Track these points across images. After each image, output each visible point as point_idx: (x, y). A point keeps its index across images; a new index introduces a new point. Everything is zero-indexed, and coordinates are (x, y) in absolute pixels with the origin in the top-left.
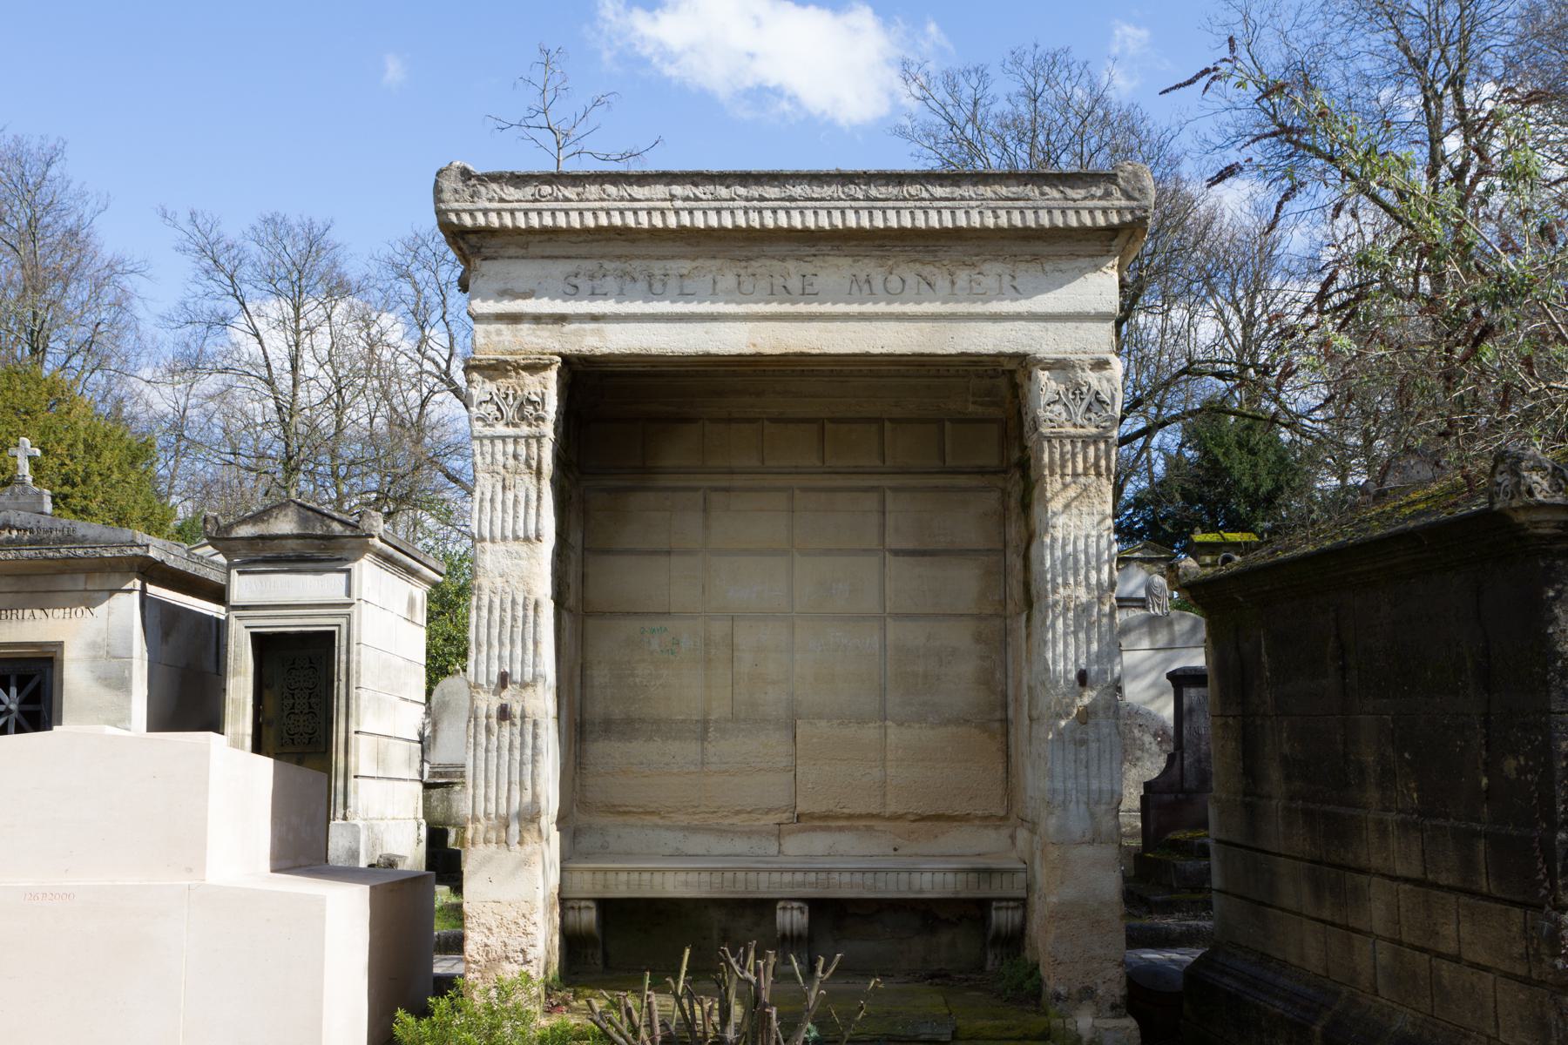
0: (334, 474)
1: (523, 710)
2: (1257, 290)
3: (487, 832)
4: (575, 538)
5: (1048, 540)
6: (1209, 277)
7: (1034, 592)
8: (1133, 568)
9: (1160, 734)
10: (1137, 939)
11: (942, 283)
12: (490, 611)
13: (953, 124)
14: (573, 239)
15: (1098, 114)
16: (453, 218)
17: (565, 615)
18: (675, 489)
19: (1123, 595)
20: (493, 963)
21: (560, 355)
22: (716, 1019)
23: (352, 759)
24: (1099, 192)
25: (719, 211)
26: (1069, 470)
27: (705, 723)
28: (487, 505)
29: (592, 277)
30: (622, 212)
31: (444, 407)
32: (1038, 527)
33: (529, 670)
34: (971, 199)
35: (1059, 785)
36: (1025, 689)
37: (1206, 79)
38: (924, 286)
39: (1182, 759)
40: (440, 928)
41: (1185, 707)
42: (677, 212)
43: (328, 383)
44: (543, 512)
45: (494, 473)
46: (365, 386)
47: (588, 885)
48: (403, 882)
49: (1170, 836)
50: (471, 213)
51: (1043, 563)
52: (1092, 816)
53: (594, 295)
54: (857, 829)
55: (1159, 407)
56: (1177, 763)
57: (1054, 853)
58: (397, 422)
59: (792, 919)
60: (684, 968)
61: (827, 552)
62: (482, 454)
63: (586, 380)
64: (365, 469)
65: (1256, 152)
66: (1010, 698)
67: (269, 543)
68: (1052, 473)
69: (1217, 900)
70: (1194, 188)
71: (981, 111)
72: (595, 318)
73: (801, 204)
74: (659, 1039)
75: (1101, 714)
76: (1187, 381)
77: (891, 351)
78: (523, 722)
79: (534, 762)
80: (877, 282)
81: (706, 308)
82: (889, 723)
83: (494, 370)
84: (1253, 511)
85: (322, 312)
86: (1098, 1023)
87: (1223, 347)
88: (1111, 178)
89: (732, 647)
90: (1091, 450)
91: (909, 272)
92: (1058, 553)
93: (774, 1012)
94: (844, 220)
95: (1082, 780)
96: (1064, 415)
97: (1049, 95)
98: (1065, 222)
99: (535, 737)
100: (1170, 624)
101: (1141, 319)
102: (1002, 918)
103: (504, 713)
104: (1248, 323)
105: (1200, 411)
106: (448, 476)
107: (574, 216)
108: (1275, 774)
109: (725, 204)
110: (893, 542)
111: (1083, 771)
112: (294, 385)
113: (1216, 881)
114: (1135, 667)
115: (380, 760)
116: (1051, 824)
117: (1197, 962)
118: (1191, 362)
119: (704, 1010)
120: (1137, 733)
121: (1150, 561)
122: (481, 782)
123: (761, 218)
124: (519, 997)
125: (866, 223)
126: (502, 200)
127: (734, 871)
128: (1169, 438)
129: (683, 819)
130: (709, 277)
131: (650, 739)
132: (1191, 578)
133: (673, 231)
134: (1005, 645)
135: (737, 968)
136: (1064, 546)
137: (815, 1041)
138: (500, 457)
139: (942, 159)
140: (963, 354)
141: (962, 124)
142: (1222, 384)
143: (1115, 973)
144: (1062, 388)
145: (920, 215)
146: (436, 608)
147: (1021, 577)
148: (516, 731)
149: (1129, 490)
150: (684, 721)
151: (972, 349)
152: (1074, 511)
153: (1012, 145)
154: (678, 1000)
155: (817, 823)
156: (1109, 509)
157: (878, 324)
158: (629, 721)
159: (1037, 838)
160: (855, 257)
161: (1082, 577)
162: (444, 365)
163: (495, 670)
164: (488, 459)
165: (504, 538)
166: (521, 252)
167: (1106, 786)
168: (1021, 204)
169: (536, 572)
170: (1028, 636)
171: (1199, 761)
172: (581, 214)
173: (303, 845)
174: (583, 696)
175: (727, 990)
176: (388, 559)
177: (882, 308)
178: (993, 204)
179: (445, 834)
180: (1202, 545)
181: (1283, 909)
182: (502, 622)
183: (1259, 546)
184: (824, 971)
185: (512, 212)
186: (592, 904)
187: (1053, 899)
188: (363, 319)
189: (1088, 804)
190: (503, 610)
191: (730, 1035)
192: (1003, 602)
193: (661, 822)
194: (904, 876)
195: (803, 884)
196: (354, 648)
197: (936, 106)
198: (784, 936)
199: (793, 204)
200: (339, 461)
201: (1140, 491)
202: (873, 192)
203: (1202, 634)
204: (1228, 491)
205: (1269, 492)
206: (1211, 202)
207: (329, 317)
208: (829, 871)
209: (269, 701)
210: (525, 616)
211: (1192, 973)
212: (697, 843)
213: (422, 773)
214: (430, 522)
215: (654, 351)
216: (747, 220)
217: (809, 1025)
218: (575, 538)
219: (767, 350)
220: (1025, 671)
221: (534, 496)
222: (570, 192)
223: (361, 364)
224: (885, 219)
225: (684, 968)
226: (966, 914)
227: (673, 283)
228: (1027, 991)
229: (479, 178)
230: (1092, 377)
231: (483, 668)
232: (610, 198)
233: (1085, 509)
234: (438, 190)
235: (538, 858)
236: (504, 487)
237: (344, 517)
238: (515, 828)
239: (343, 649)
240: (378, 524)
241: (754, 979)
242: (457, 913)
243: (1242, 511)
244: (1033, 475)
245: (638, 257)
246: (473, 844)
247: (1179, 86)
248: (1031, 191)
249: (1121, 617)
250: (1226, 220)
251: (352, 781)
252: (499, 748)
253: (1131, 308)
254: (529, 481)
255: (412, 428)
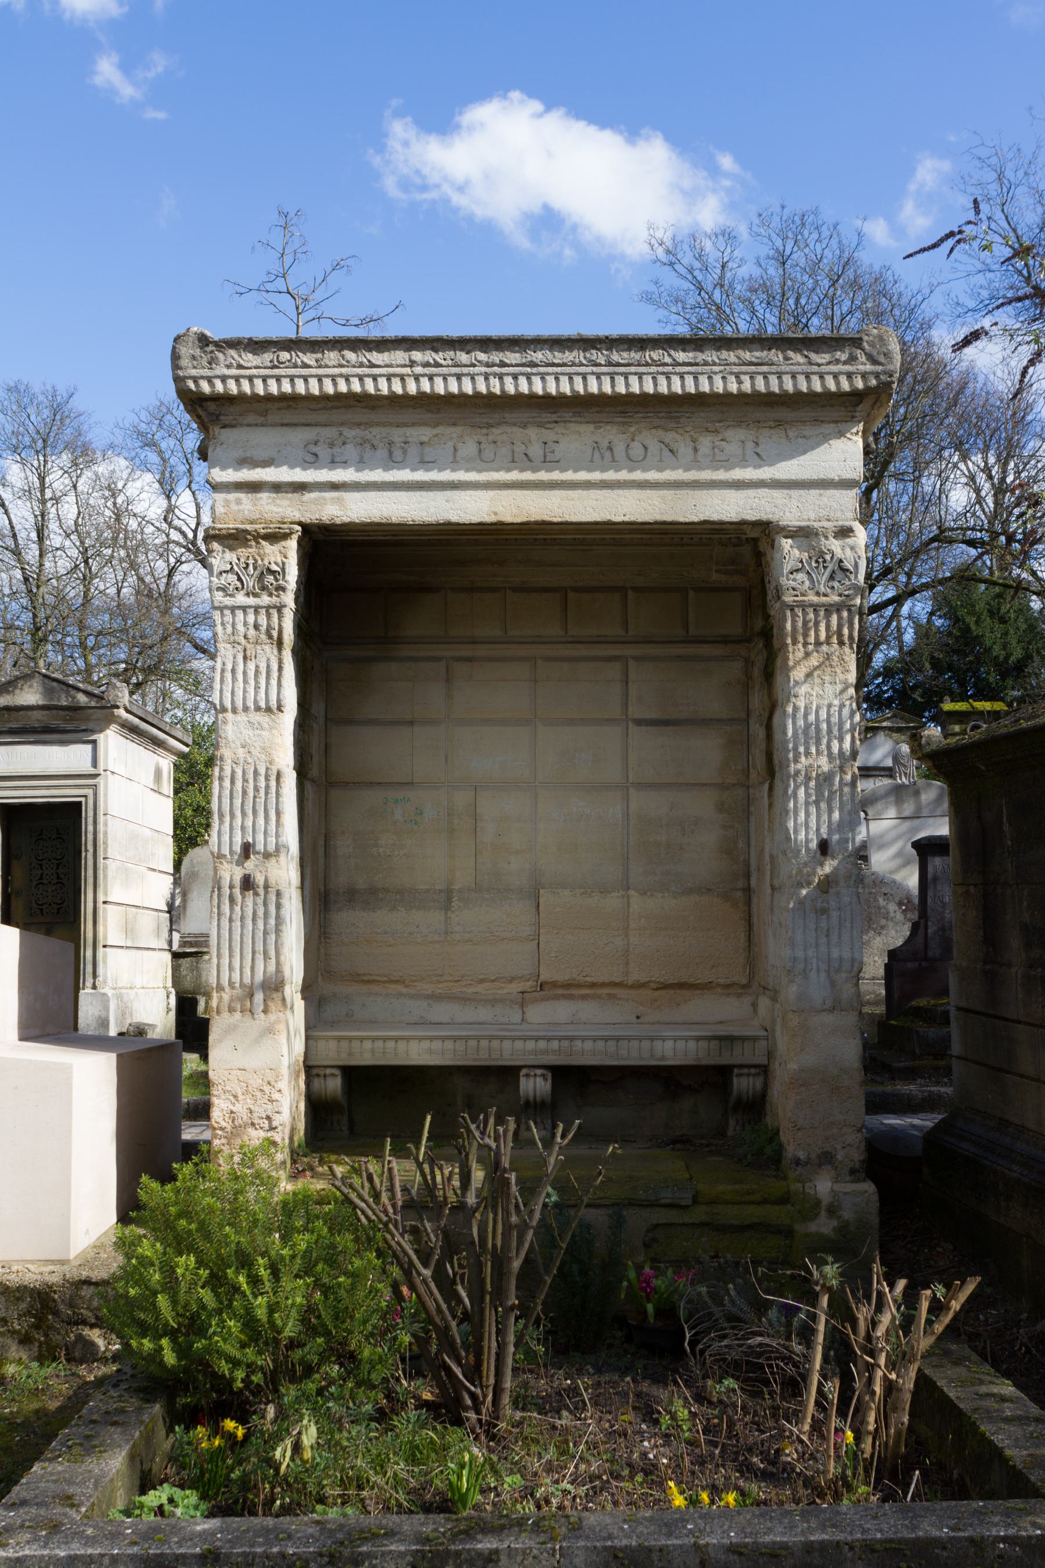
0: (83, 645)
1: (266, 880)
2: (1009, 457)
3: (232, 1000)
4: (318, 708)
5: (790, 709)
6: (961, 443)
7: (776, 761)
8: (881, 737)
9: (905, 902)
10: (876, 1105)
11: (685, 449)
12: (233, 782)
13: (701, 289)
14: (313, 406)
15: (844, 274)
16: (191, 385)
17: (308, 786)
18: (417, 659)
19: (870, 764)
20: (237, 1130)
21: (300, 524)
22: (456, 1183)
23: (101, 929)
24: (844, 357)
25: (459, 377)
26: (812, 639)
27: (448, 893)
28: (228, 675)
29: (332, 445)
30: (361, 378)
31: (193, 578)
32: (780, 697)
33: (272, 840)
34: (714, 364)
35: (800, 954)
36: (767, 858)
37: (951, 242)
38: (666, 453)
39: (926, 927)
40: (187, 1095)
41: (930, 876)
42: (417, 378)
43: (74, 553)
44: (284, 682)
45: (235, 643)
46: (112, 556)
47: (334, 1052)
48: (150, 1050)
49: (914, 1003)
50: (209, 380)
51: (785, 733)
52: (833, 983)
53: (333, 463)
54: (600, 997)
55: (909, 576)
56: (921, 931)
57: (794, 1020)
58: (144, 592)
59: (535, 1086)
60: (426, 1135)
61: (571, 722)
62: (223, 624)
63: (328, 552)
64: (113, 640)
65: (1006, 317)
66: (753, 868)
67: (14, 714)
68: (795, 642)
69: (956, 1067)
70: (945, 352)
71: (728, 275)
72: (335, 486)
73: (542, 370)
74: (400, 1203)
75: (842, 883)
76: (937, 549)
77: (633, 519)
78: (266, 893)
79: (278, 931)
80: (620, 449)
81: (446, 476)
82: (632, 892)
83: (234, 539)
84: (1003, 679)
85: (67, 481)
86: (836, 1187)
87: (974, 514)
88: (856, 342)
89: (475, 817)
90: (834, 618)
91: (651, 439)
92: (801, 723)
93: (513, 1177)
94: (585, 386)
95: (823, 949)
96: (807, 583)
97: (799, 257)
98: (809, 387)
99: (278, 906)
100: (917, 793)
101: (892, 486)
102: (743, 1085)
103: (247, 883)
104: (1000, 490)
105: (950, 578)
106: (196, 647)
107: (313, 383)
108: (1015, 942)
109: (465, 370)
110: (635, 711)
111: (823, 940)
112: (41, 556)
113: (956, 1048)
114: (882, 836)
115: (128, 929)
116: (791, 992)
117: (937, 1127)
118: (942, 530)
119: (446, 1175)
120: (881, 901)
121: (899, 730)
122: (225, 952)
123: (502, 384)
124: (263, 1163)
125: (607, 389)
126: (240, 367)
127: (478, 1039)
128: (919, 607)
129: (427, 988)
130: (450, 444)
131: (394, 908)
132: (934, 747)
133: (413, 397)
134: (748, 814)
135: (477, 1134)
136: (806, 716)
137: (556, 1205)
138: (240, 628)
139: (690, 324)
140: (705, 522)
141: (710, 288)
142: (973, 552)
143: (854, 1138)
144: (805, 556)
145: (662, 381)
146: (185, 779)
147: (763, 746)
148: (260, 900)
149: (878, 659)
150: (427, 891)
151: (715, 517)
152: (817, 680)
153: (760, 309)
154: (420, 1165)
155: (560, 991)
156: (852, 677)
157: (620, 492)
158: (373, 891)
159: (778, 1006)
160: (597, 423)
161: (824, 747)
162: (190, 535)
163: (238, 840)
164: (229, 630)
165: (246, 709)
166: (261, 420)
167: (846, 955)
168: (765, 369)
169: (280, 743)
170: (771, 805)
171: (943, 929)
172: (320, 380)
173: (52, 1012)
174: (326, 866)
175: (467, 1155)
176: (133, 730)
177: (623, 475)
178: (736, 369)
179: (194, 1003)
180: (951, 714)
181: (1021, 1076)
182: (245, 792)
183: (1007, 713)
184: (563, 1137)
185: (250, 379)
186: (337, 1072)
187: (793, 1066)
188: (109, 488)
189: (828, 972)
190: (245, 780)
191: (471, 1200)
192: (746, 772)
193: (404, 990)
194: (646, 1044)
195: (546, 1052)
196: (101, 819)
197: (683, 271)
198: (527, 1103)
199: (535, 370)
200: (86, 633)
201: (890, 660)
202: (615, 357)
203: (946, 805)
204: (978, 661)
205: (1019, 661)
206: (964, 365)
207: (75, 487)
208: (572, 1039)
209: (18, 871)
210: (267, 787)
211: (931, 1137)
212: (442, 1012)
213: (170, 943)
214: (179, 693)
215: (394, 520)
216: (488, 386)
217: (550, 1189)
218: (318, 708)
219: (508, 518)
220: (767, 840)
221: (275, 667)
222: (309, 358)
223: (108, 534)
224: (627, 385)
225: (426, 1135)
226: (707, 1080)
227: (413, 451)
228: (769, 1157)
229: (217, 344)
230: (835, 545)
231: (226, 838)
232: (349, 364)
233: (827, 678)
234: (175, 357)
235: (282, 1027)
236: (245, 658)
237: (90, 688)
238: (259, 997)
239: (90, 820)
240: (123, 695)
241: (494, 1145)
242: (203, 1080)
243: (991, 680)
244: (776, 644)
245: (378, 424)
246: (218, 1012)
247: (916, 253)
248: (775, 355)
249: (865, 786)
250: (979, 385)
251: (101, 951)
252: (242, 918)
253: (881, 475)
254: (269, 651)
255: (159, 598)
